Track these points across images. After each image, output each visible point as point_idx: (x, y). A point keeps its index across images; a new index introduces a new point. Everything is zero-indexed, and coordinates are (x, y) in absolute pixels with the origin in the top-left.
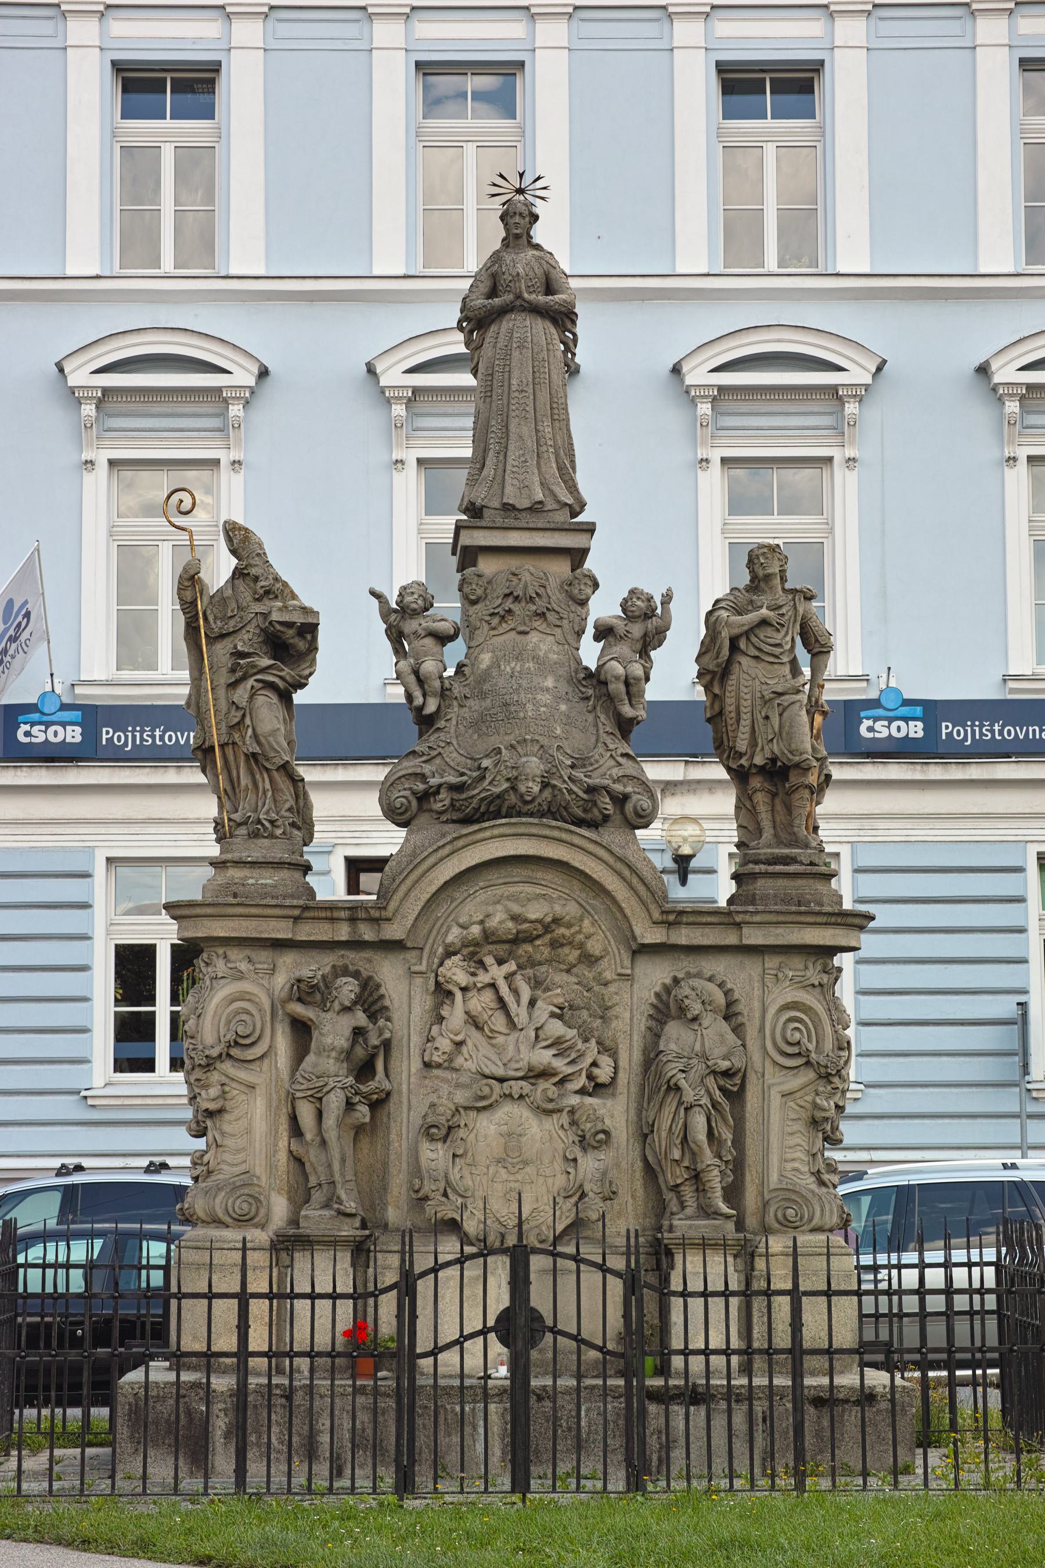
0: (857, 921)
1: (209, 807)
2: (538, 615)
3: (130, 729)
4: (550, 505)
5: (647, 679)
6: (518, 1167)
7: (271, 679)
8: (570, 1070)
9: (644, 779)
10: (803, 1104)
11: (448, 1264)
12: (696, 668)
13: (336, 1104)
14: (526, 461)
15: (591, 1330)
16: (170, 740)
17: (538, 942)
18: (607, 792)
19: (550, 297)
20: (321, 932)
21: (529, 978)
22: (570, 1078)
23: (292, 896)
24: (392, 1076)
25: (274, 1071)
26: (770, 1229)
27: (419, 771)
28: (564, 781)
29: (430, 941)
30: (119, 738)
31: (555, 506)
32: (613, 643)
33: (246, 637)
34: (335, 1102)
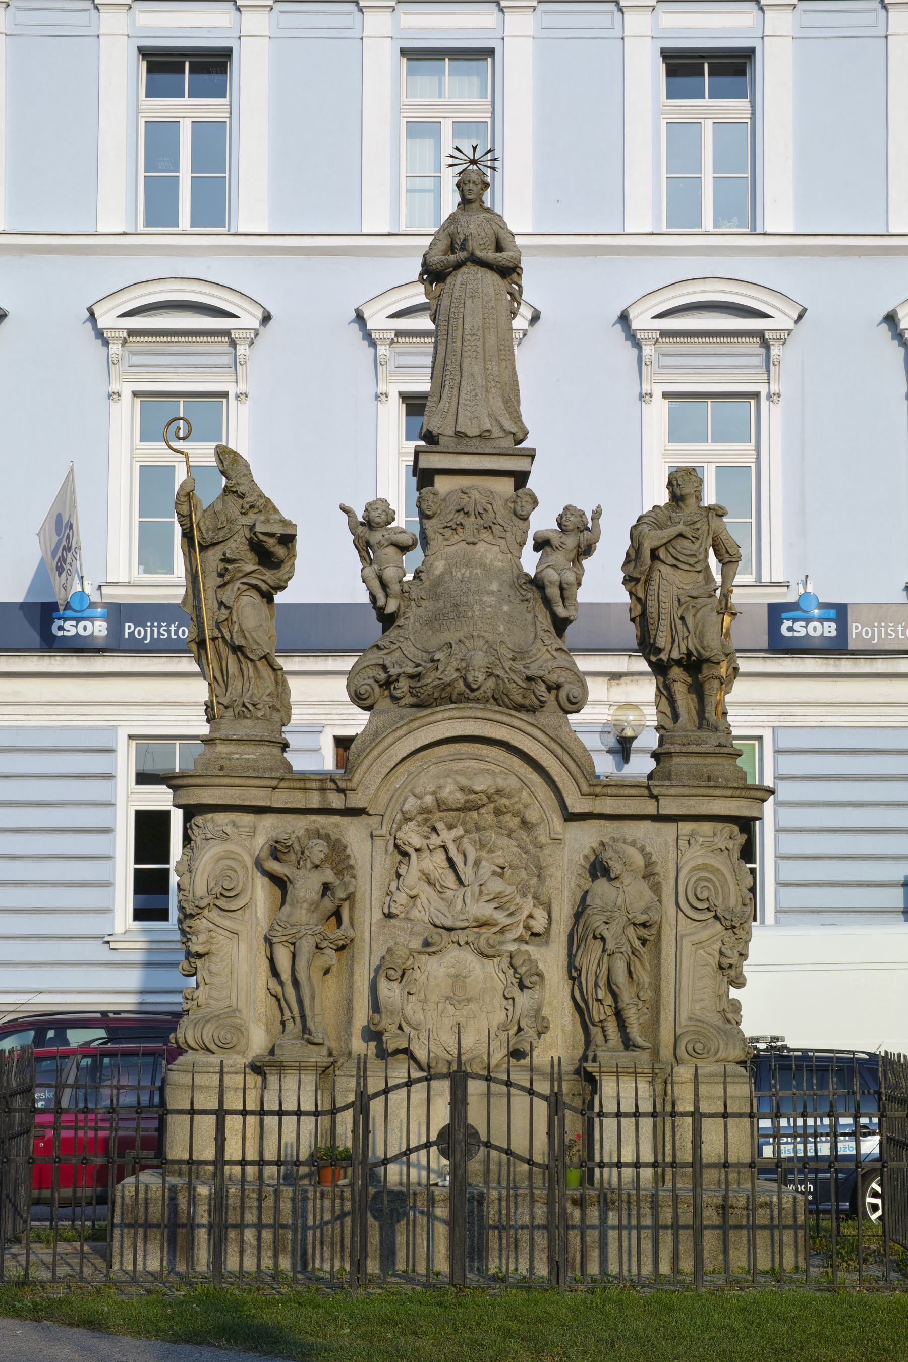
0: (759, 794)
1: (200, 690)
2: (485, 528)
3: (149, 624)
4: (497, 432)
5: (579, 584)
6: (463, 1004)
7: (254, 582)
8: (508, 921)
9: (575, 671)
10: (711, 951)
11: (397, 1087)
12: (622, 575)
13: (307, 948)
14: (476, 396)
15: (519, 1145)
16: (183, 634)
17: (482, 810)
18: (543, 681)
19: (499, 254)
20: (297, 800)
21: (475, 842)
22: (508, 928)
23: (271, 769)
24: (356, 925)
25: (254, 920)
26: (681, 1060)
27: (381, 662)
28: (506, 672)
29: (390, 809)
30: (139, 632)
31: (501, 434)
32: (549, 553)
33: (234, 546)
34: (306, 946)
